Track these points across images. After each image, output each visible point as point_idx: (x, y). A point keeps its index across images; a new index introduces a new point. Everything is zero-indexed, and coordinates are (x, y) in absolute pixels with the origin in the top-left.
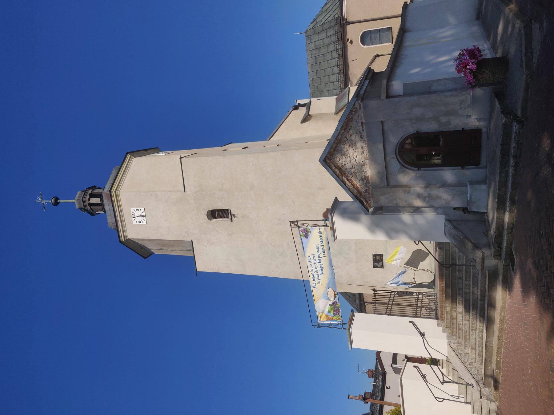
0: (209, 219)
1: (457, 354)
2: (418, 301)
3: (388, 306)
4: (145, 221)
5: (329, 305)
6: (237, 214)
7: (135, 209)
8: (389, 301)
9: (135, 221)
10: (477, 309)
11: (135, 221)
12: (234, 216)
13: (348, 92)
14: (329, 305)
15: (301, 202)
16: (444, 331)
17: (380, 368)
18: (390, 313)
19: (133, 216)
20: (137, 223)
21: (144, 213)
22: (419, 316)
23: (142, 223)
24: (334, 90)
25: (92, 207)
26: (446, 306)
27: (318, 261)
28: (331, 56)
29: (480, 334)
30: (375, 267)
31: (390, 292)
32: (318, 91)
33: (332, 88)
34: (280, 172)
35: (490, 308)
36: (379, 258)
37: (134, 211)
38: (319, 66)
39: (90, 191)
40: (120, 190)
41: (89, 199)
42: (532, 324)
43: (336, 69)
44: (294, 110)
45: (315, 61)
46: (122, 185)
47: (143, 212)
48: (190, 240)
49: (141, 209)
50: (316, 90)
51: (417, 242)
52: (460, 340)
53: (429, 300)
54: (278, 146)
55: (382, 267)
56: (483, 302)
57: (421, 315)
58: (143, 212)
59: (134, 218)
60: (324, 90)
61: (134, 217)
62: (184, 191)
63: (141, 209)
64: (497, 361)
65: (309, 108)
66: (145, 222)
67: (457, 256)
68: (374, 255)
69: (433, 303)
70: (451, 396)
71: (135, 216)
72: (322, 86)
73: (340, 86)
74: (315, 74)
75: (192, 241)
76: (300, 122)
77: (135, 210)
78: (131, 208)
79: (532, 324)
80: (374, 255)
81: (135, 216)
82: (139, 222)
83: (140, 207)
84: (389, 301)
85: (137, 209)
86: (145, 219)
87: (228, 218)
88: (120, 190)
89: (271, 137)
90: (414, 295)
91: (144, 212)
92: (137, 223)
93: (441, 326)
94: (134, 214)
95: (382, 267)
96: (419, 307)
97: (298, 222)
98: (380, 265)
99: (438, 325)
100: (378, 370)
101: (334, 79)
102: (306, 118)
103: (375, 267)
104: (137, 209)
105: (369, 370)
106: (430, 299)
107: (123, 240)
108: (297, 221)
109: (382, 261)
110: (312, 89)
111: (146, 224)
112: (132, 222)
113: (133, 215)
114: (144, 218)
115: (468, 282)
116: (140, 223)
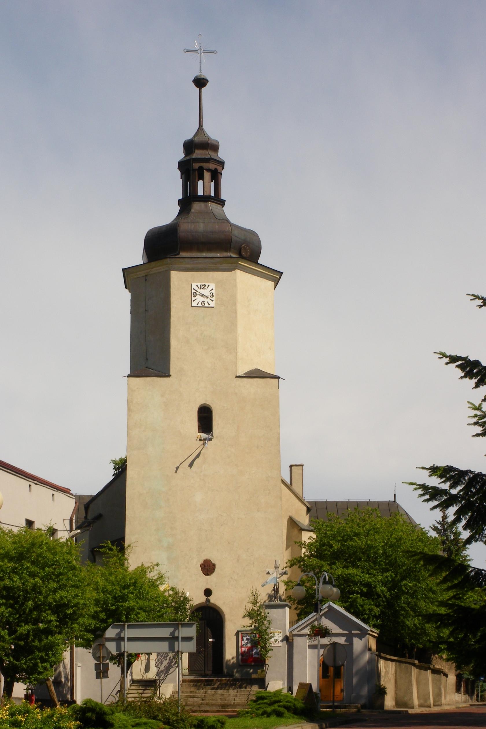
7: (213, 291)
19: (203, 286)
21: (208, 306)
35: (336, 679)
37: (210, 288)
41: (209, 170)
47: (209, 305)
48: (171, 374)
56: (410, 606)
58: (209, 305)
59: (201, 286)
61: (202, 287)
65: (138, 267)
66: (194, 304)
70: (115, 698)
71: (203, 289)
76: (291, 515)
77: (212, 291)
78: (354, 638)
81: (203, 289)
85: (214, 295)
86: (198, 306)
89: (131, 694)
102: (297, 525)
104: (212, 295)
111: (193, 305)
112: (194, 282)
116: (193, 296)
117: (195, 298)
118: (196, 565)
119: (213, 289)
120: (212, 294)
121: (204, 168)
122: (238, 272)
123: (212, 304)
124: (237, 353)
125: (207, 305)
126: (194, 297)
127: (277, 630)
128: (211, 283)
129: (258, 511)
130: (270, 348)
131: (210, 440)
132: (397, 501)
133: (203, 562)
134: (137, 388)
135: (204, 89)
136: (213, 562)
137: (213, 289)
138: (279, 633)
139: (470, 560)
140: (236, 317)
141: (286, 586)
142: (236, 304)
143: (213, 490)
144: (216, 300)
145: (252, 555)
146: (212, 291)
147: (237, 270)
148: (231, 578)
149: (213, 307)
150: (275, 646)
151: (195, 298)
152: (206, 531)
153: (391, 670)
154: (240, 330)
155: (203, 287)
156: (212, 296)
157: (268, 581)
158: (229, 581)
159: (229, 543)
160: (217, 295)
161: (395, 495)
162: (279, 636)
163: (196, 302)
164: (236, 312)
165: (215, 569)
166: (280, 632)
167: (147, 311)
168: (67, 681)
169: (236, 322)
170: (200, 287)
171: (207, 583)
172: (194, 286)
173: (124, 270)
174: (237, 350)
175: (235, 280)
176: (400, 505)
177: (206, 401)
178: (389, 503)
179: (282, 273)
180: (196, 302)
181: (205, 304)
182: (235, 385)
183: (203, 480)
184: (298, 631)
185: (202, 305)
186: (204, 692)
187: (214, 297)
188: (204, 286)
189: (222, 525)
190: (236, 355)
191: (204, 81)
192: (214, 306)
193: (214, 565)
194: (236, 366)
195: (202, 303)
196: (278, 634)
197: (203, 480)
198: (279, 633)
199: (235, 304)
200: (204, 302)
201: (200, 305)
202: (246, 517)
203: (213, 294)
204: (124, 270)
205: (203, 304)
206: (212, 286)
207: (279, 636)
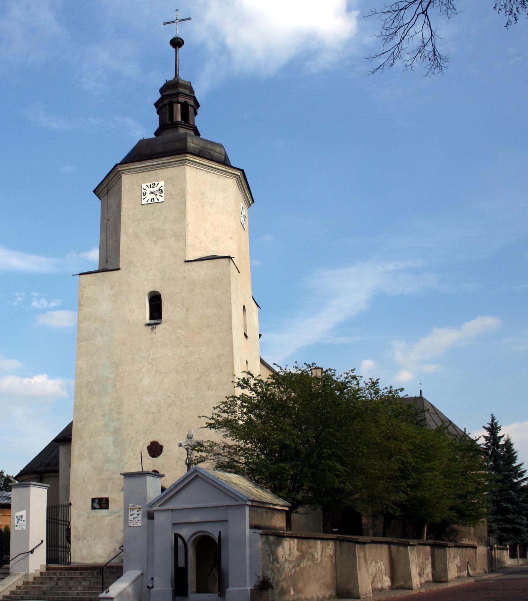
2: (62, 547)
3: (60, 524)
8: (60, 520)
9: (146, 188)
10: (498, 561)
11: (146, 188)
12: (152, 329)
18: (49, 522)
19: (153, 184)
20: (143, 191)
22: (48, 549)
23: (143, 197)
25: (167, 106)
30: (93, 500)
31: (69, 521)
36: (104, 505)
40: (189, 166)
42: (349, 470)
46: (195, 168)
47: (158, 200)
48: (120, 267)
49: (162, 196)
51: (122, 548)
52: (87, 589)
53: (64, 558)
54: (246, 362)
55: (93, 508)
57: (49, 550)
58: (158, 200)
59: (150, 185)
61: (152, 186)
62: (187, 260)
63: (162, 196)
66: (144, 202)
67: (111, 581)
68: (107, 499)
69: (61, 562)
75: (119, 269)
79: (349, 470)
80: (107, 499)
81: (153, 187)
82: (144, 193)
84: (60, 520)
85: (163, 191)
86: (148, 203)
87: (151, 318)
88: (189, 166)
90: (68, 544)
91: (159, 201)
92: (143, 191)
93: (41, 568)
95: (93, 508)
98: (96, 505)
99: (42, 566)
103: (93, 500)
106: (64, 559)
107: (119, 169)
109: (101, 508)
111: (142, 204)
112: (145, 183)
113: (155, 184)
114: (149, 202)
115: (87, 589)
116: (143, 195)
118: (142, 447)
119: (162, 186)
120: (161, 190)
121: (174, 101)
123: (161, 199)
124: (185, 240)
125: (156, 201)
126: (144, 195)
127: (136, 506)
128: (161, 181)
129: (208, 389)
130: (231, 238)
131: (159, 323)
132: (423, 396)
133: (149, 444)
134: (88, 284)
135: (181, 50)
136: (160, 444)
137: (162, 186)
138: (138, 510)
139: (516, 452)
140: (185, 207)
142: (185, 196)
143: (161, 372)
144: (165, 195)
145: (202, 434)
146: (161, 188)
148: (179, 458)
149: (163, 202)
150: (134, 526)
152: (153, 413)
154: (190, 218)
155: (153, 186)
156: (161, 193)
158: (177, 461)
159: (177, 424)
160: (166, 190)
161: (421, 391)
162: (138, 513)
163: (146, 200)
164: (185, 203)
165: (162, 451)
166: (140, 508)
167: (109, 220)
169: (185, 211)
170: (149, 187)
171: (154, 465)
172: (144, 186)
173: (95, 191)
174: (185, 237)
175: (185, 175)
176: (426, 399)
177: (155, 288)
178: (415, 399)
180: (146, 200)
181: (154, 200)
182: (184, 270)
183: (151, 364)
184: (159, 506)
185: (151, 201)
186: (55, 584)
187: (163, 192)
188: (154, 184)
189: (170, 406)
190: (185, 242)
191: (179, 40)
192: (163, 201)
193: (161, 447)
194: (185, 252)
196: (138, 511)
198: (138, 510)
200: (153, 198)
201: (149, 202)
202: (195, 397)
203: (162, 190)
204: (95, 191)
205: (153, 201)
206: (162, 183)
207: (138, 513)
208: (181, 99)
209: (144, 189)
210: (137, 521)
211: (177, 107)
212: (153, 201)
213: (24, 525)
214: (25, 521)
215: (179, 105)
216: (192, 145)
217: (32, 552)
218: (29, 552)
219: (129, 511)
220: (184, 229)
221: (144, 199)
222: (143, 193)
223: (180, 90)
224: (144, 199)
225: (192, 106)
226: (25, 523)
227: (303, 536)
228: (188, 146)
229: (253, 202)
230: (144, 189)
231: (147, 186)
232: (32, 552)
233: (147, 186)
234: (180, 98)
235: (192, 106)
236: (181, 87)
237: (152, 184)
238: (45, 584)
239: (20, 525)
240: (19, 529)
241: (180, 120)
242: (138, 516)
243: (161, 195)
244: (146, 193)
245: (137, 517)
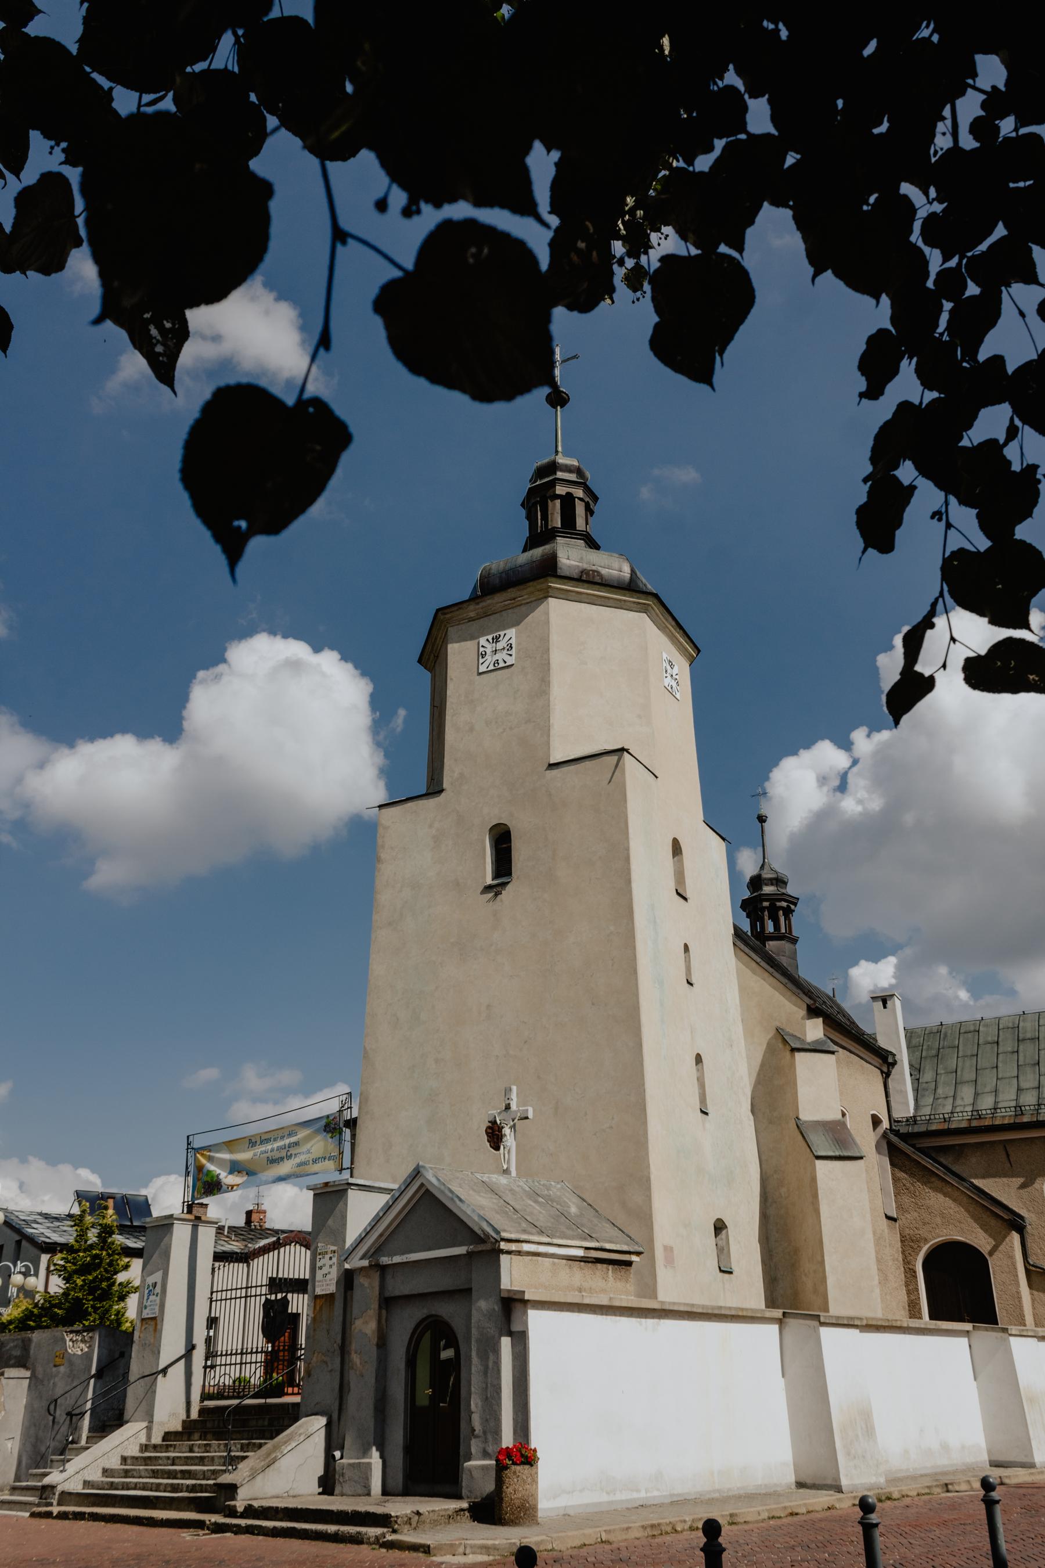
0: (491, 829)
1: (126, 1443)
4: (485, 670)
5: (220, 1174)
6: (501, 901)
13: (846, 1154)
14: (220, 1174)
15: (528, 1059)
16: (535, 1450)
17: (262, 1243)
21: (504, 665)
24: (932, 1099)
26: (214, 1420)
27: (289, 1154)
28: (1028, 1087)
29: (141, 1484)
32: (943, 1048)
33: (940, 1091)
34: (593, 1004)
38: (1010, 1049)
39: (579, 493)
43: (986, 1103)
44: (807, 1004)
45: (1029, 1035)
47: (505, 662)
49: (511, 655)
50: (946, 1043)
58: (505, 662)
59: (493, 639)
60: (940, 1066)
63: (511, 655)
64: (85, 1513)
66: (482, 669)
72: (952, 1063)
73: (923, 1118)
74: (990, 1039)
82: (483, 653)
83: (518, 651)
85: (513, 646)
86: (489, 669)
91: (507, 664)
92: (482, 649)
94: (501, 638)
96: (281, 1360)
97: (349, 1110)
100: (260, 1238)
101: (963, 1099)
105: (265, 1212)
108: (351, 1108)
110: (950, 1032)
113: (500, 635)
116: (480, 657)
117: (484, 660)
118: (477, 1129)
122: (552, 601)
123: (510, 661)
125: (502, 665)
126: (483, 657)
141: (533, 1448)
144: (517, 653)
147: (550, 599)
151: (484, 660)
153: (639, 603)
154: (558, 691)
157: (27, 1514)
160: (518, 644)
168: (117, 1252)
169: (549, 677)
179: (798, 899)
181: (498, 664)
185: (494, 666)
195: (494, 663)
197: (494, 960)
199: (547, 650)
200: (498, 660)
201: (491, 667)
203: (511, 644)
205: (496, 665)
207: (331, 1262)
208: (560, 490)
209: (483, 646)
210: (328, 1282)
211: (554, 505)
212: (496, 665)
213: (157, 1305)
214: (159, 1295)
215: (558, 502)
216: (567, 562)
217: (164, 1371)
218: (159, 1372)
219: (318, 1260)
220: (547, 708)
221: (482, 664)
222: (482, 654)
223: (560, 475)
224: (482, 664)
225: (581, 499)
226: (158, 1299)
227: (617, 1303)
228: (559, 565)
229: (699, 651)
230: (483, 646)
231: (488, 640)
232: (164, 1371)
233: (488, 640)
234: (557, 487)
235: (581, 499)
236: (561, 471)
237: (495, 635)
238: (172, 1449)
239: (150, 1306)
240: (148, 1314)
241: (560, 526)
242: (331, 1270)
243: (509, 653)
244: (485, 652)
245: (329, 1273)
